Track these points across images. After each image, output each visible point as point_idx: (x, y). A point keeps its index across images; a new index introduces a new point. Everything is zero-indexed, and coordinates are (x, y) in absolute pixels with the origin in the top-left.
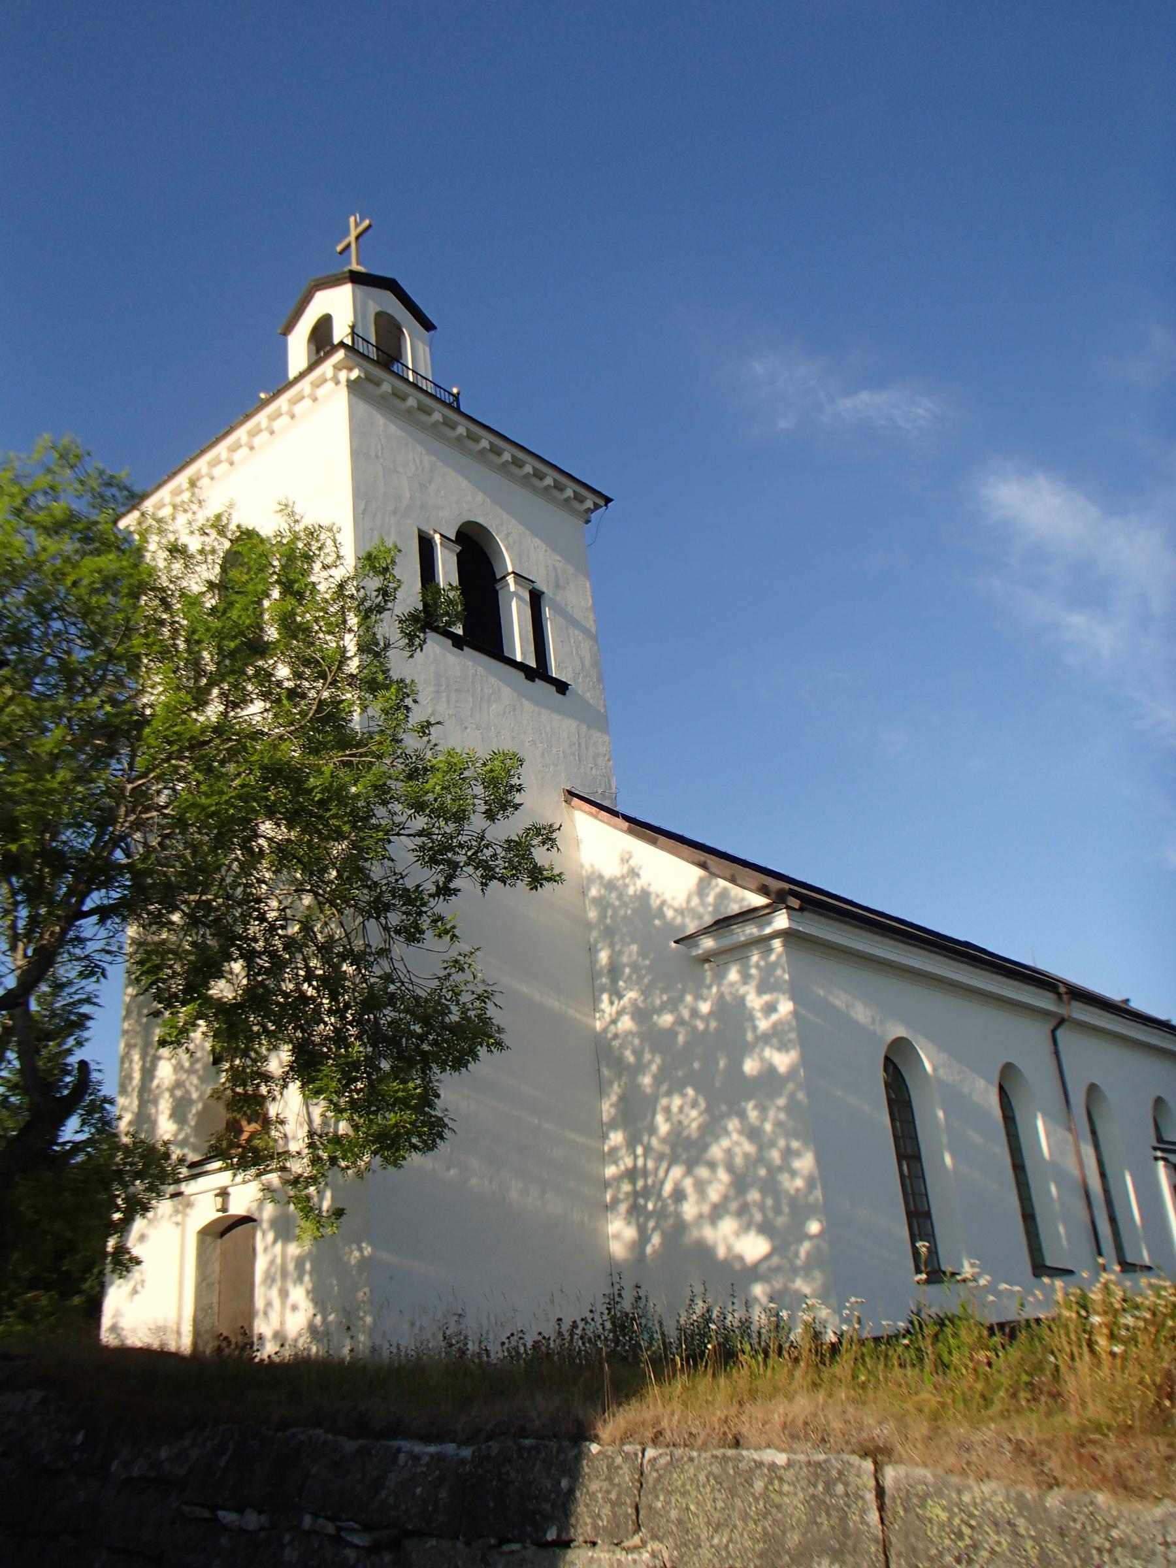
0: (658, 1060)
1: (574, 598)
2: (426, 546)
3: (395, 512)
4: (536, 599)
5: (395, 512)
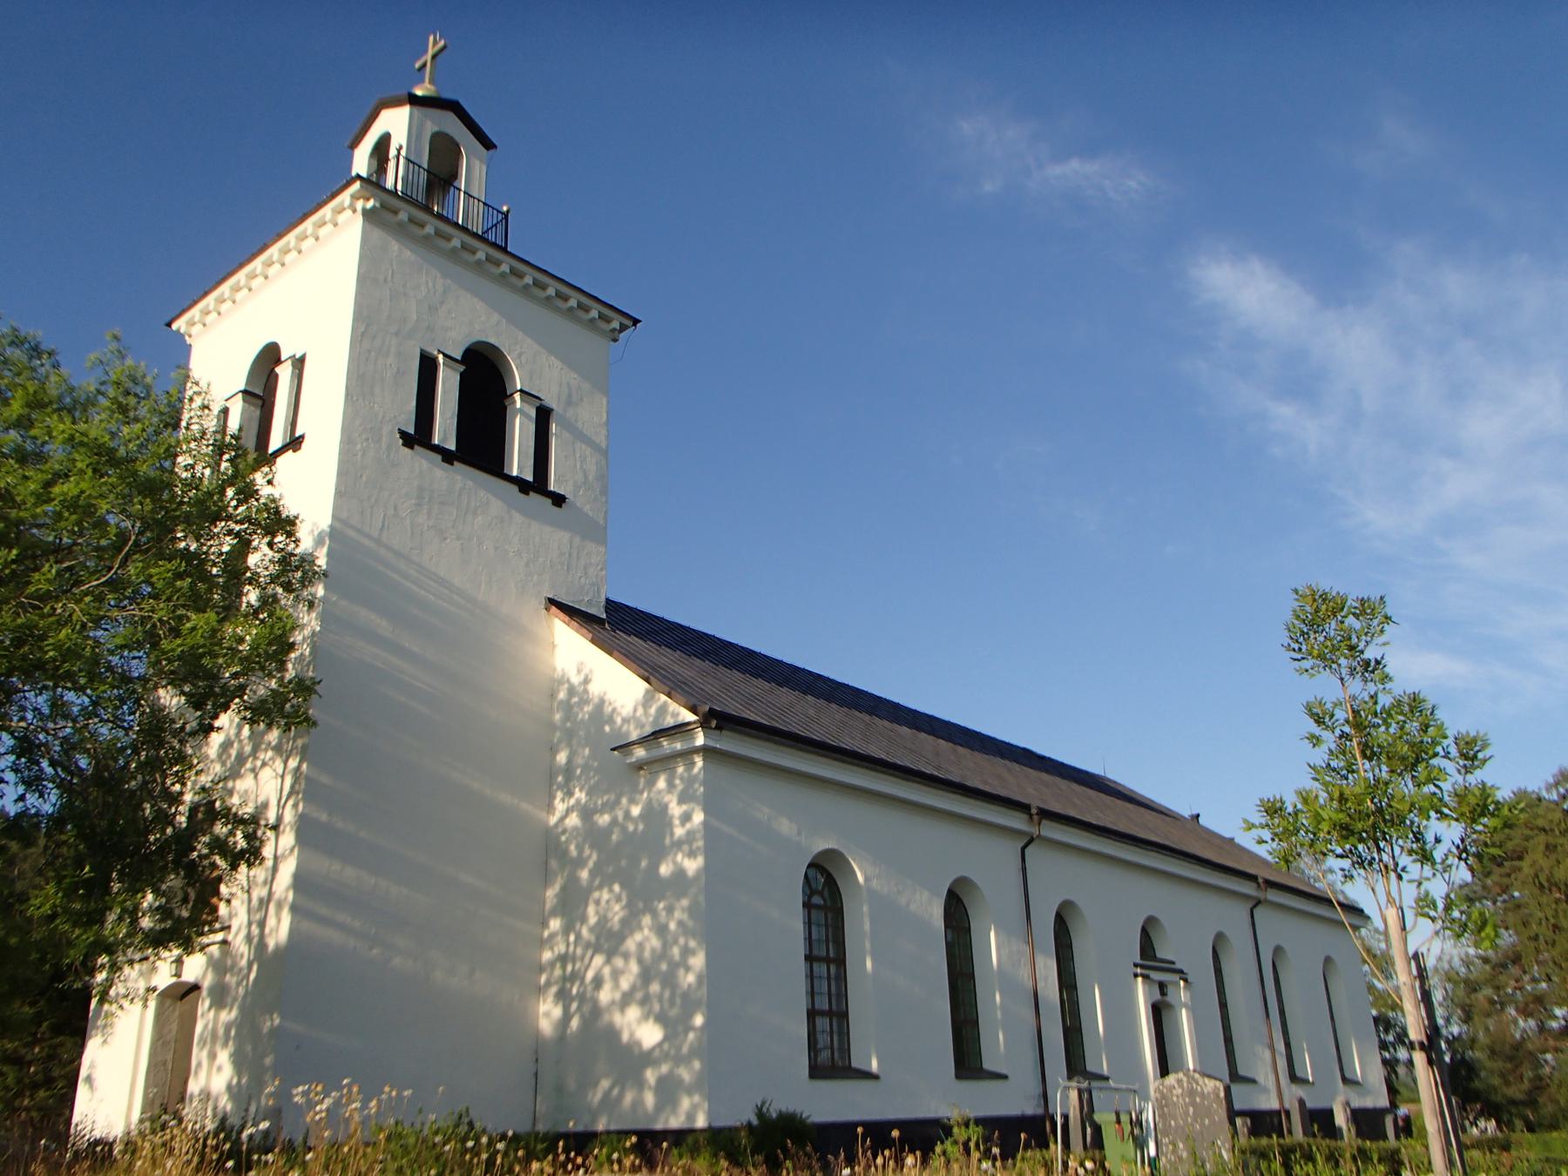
0: (595, 857)
1: (586, 417)
2: (428, 367)
3: (397, 334)
4: (543, 416)
5: (397, 334)
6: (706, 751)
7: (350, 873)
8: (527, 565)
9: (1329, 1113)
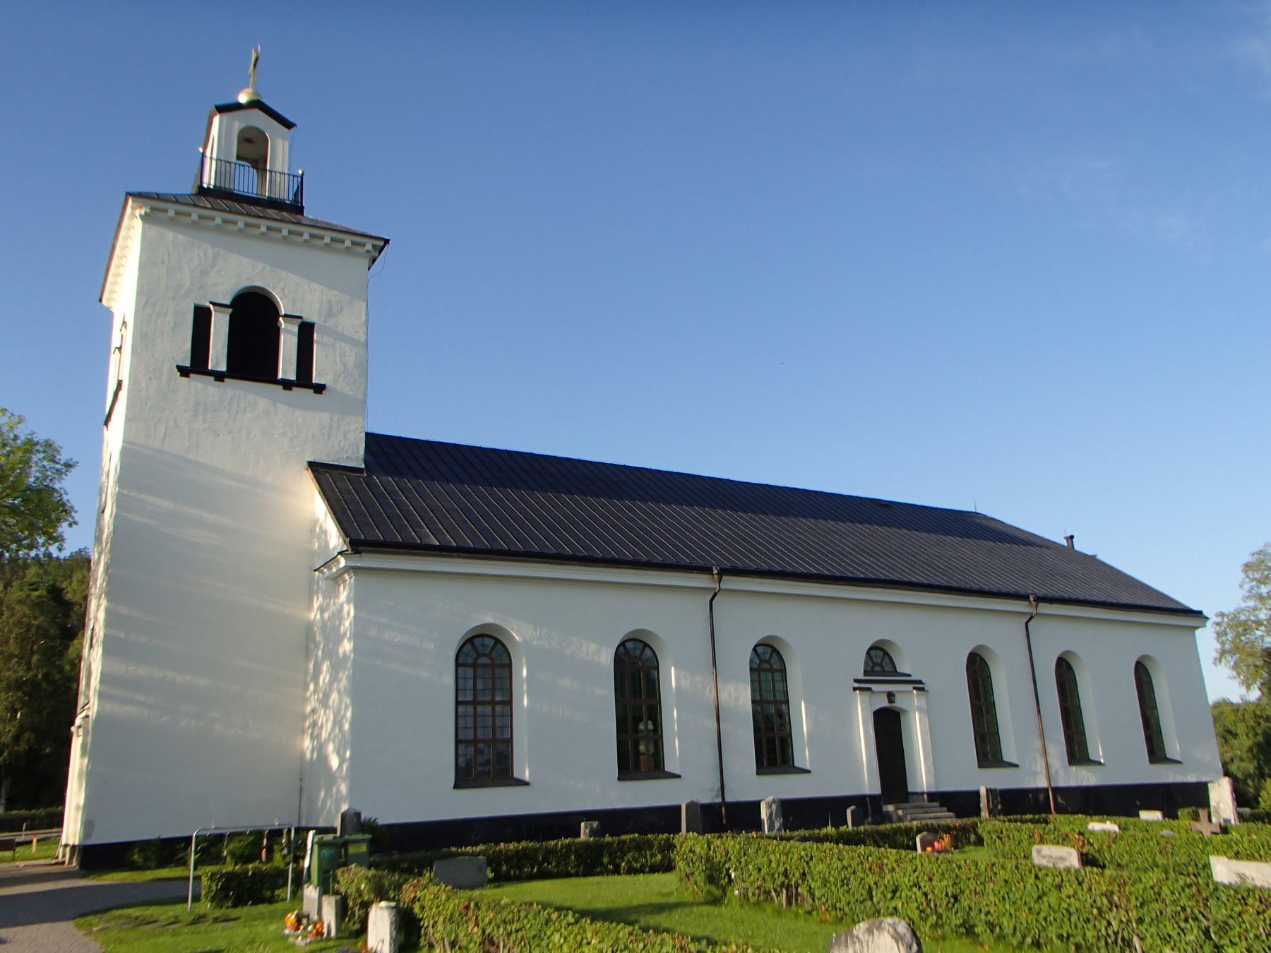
2: (202, 317)
4: (306, 331)
6: (347, 569)
7: (143, 671)
8: (291, 440)
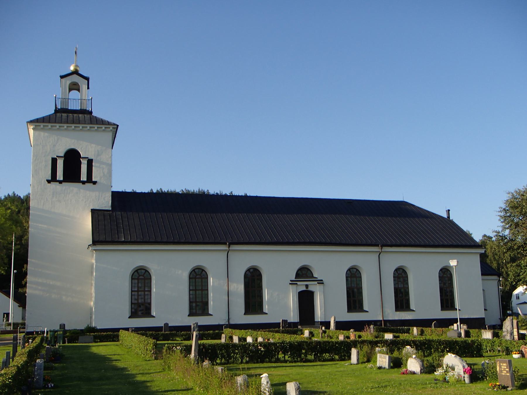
2: (54, 161)
9: (329, 323)
